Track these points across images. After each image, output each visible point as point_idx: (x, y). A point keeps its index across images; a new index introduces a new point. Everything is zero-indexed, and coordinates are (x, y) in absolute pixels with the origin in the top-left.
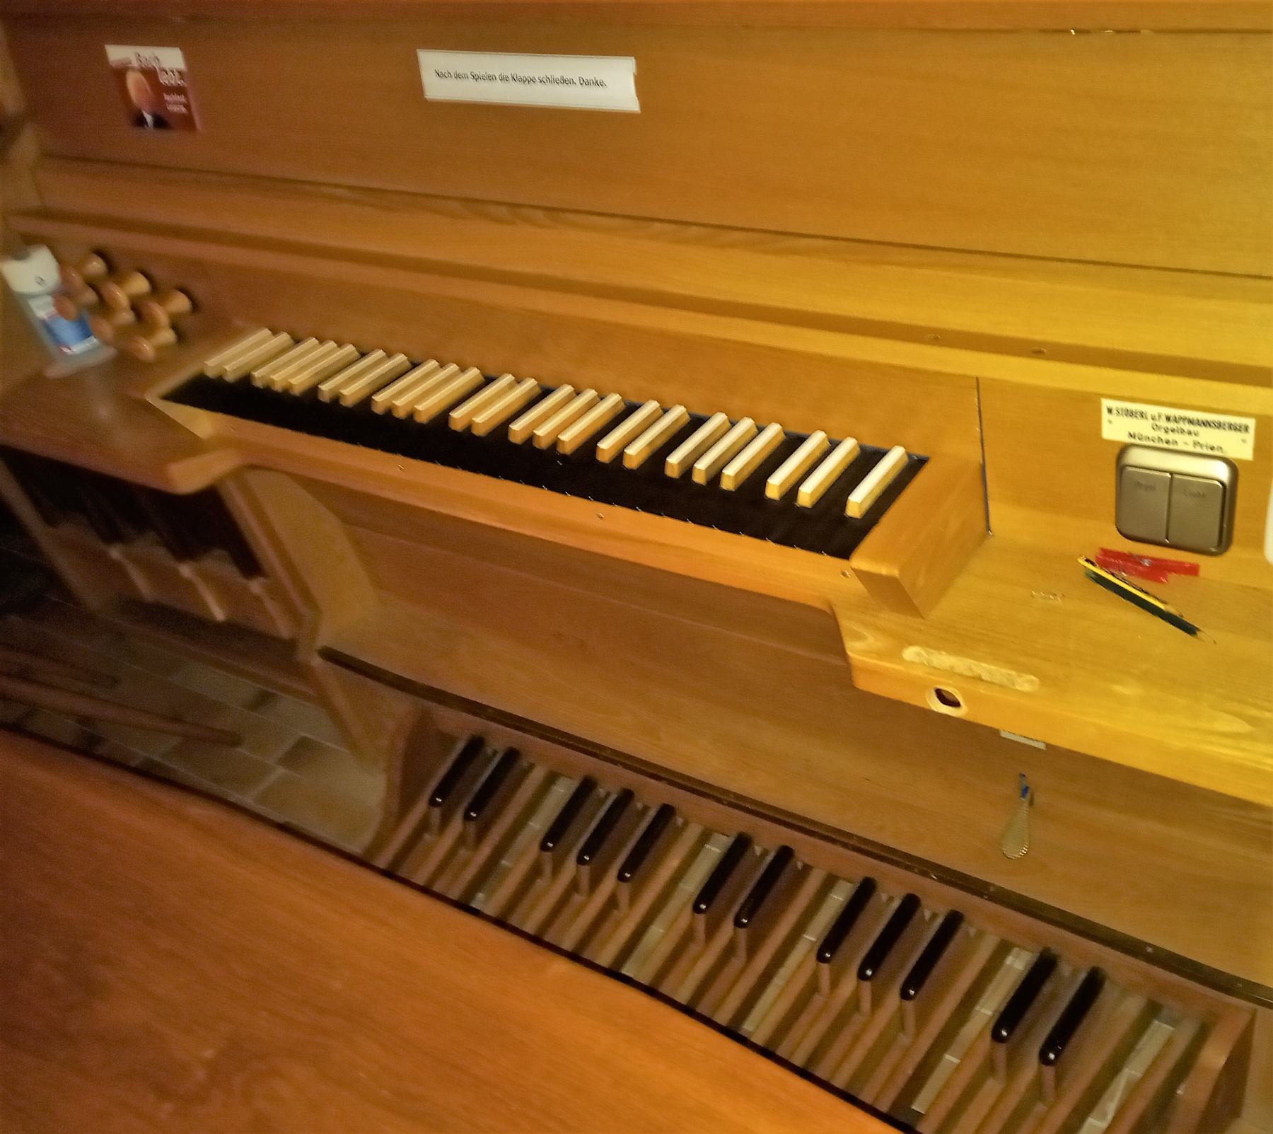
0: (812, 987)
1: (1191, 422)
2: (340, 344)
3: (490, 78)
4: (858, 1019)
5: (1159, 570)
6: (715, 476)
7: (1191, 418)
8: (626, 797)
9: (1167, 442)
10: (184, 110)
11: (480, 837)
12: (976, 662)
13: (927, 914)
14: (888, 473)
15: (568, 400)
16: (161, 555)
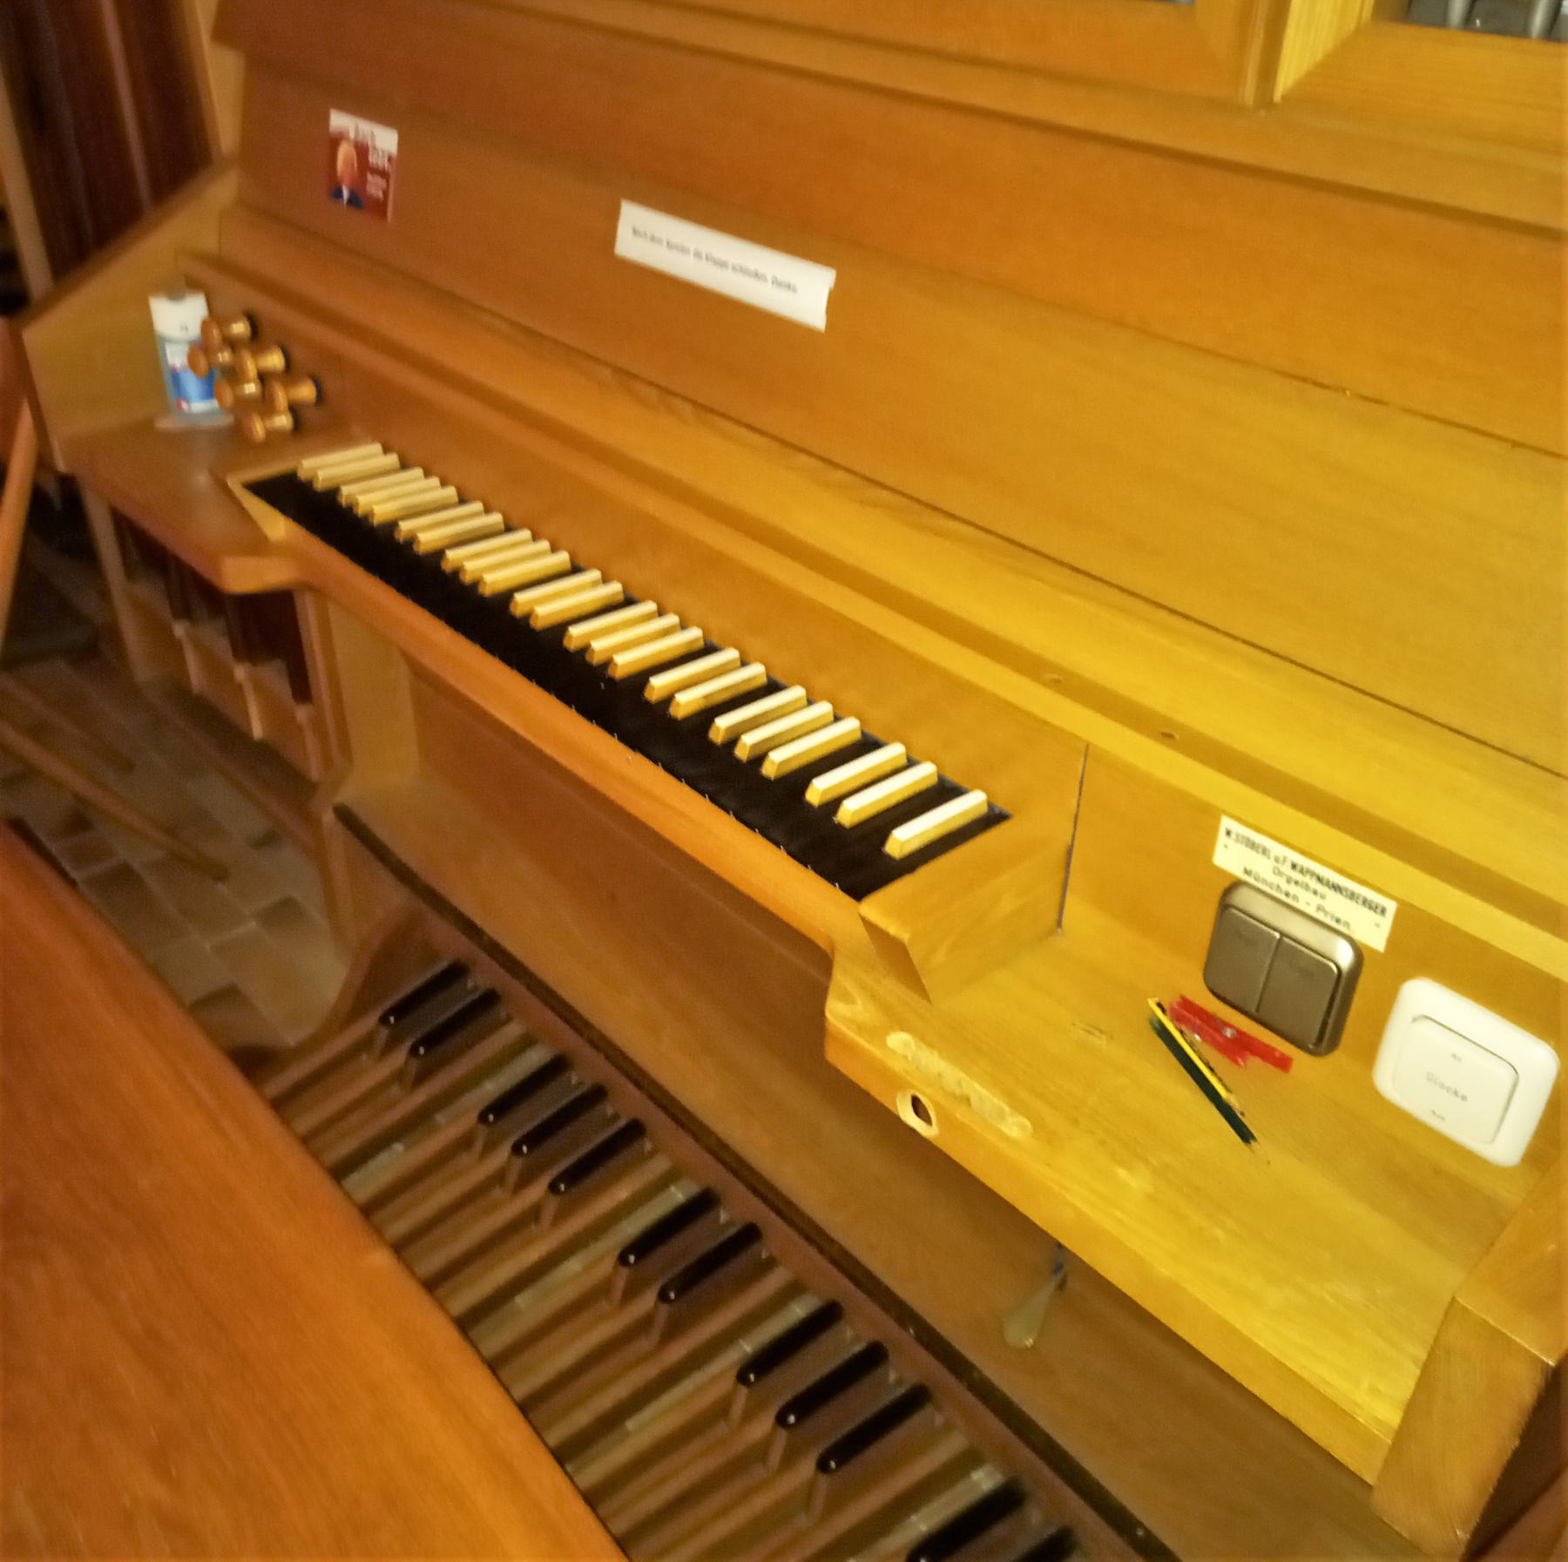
0: (721, 1410)
1: (1319, 879)
2: (444, 483)
3: (684, 250)
4: (759, 1472)
5: (1240, 1047)
6: (759, 759)
7: (1321, 875)
8: (597, 1094)
9: (1287, 894)
10: (381, 194)
11: (421, 1078)
12: (967, 1078)
13: (892, 1377)
14: (953, 818)
15: (648, 618)
16: (223, 647)
